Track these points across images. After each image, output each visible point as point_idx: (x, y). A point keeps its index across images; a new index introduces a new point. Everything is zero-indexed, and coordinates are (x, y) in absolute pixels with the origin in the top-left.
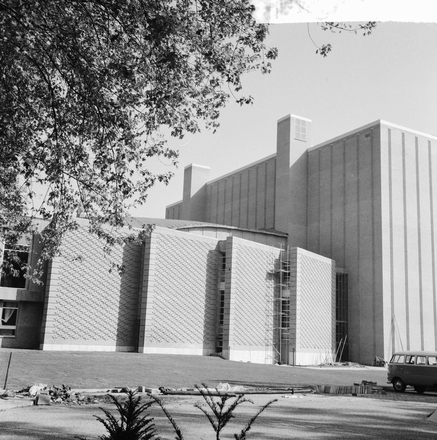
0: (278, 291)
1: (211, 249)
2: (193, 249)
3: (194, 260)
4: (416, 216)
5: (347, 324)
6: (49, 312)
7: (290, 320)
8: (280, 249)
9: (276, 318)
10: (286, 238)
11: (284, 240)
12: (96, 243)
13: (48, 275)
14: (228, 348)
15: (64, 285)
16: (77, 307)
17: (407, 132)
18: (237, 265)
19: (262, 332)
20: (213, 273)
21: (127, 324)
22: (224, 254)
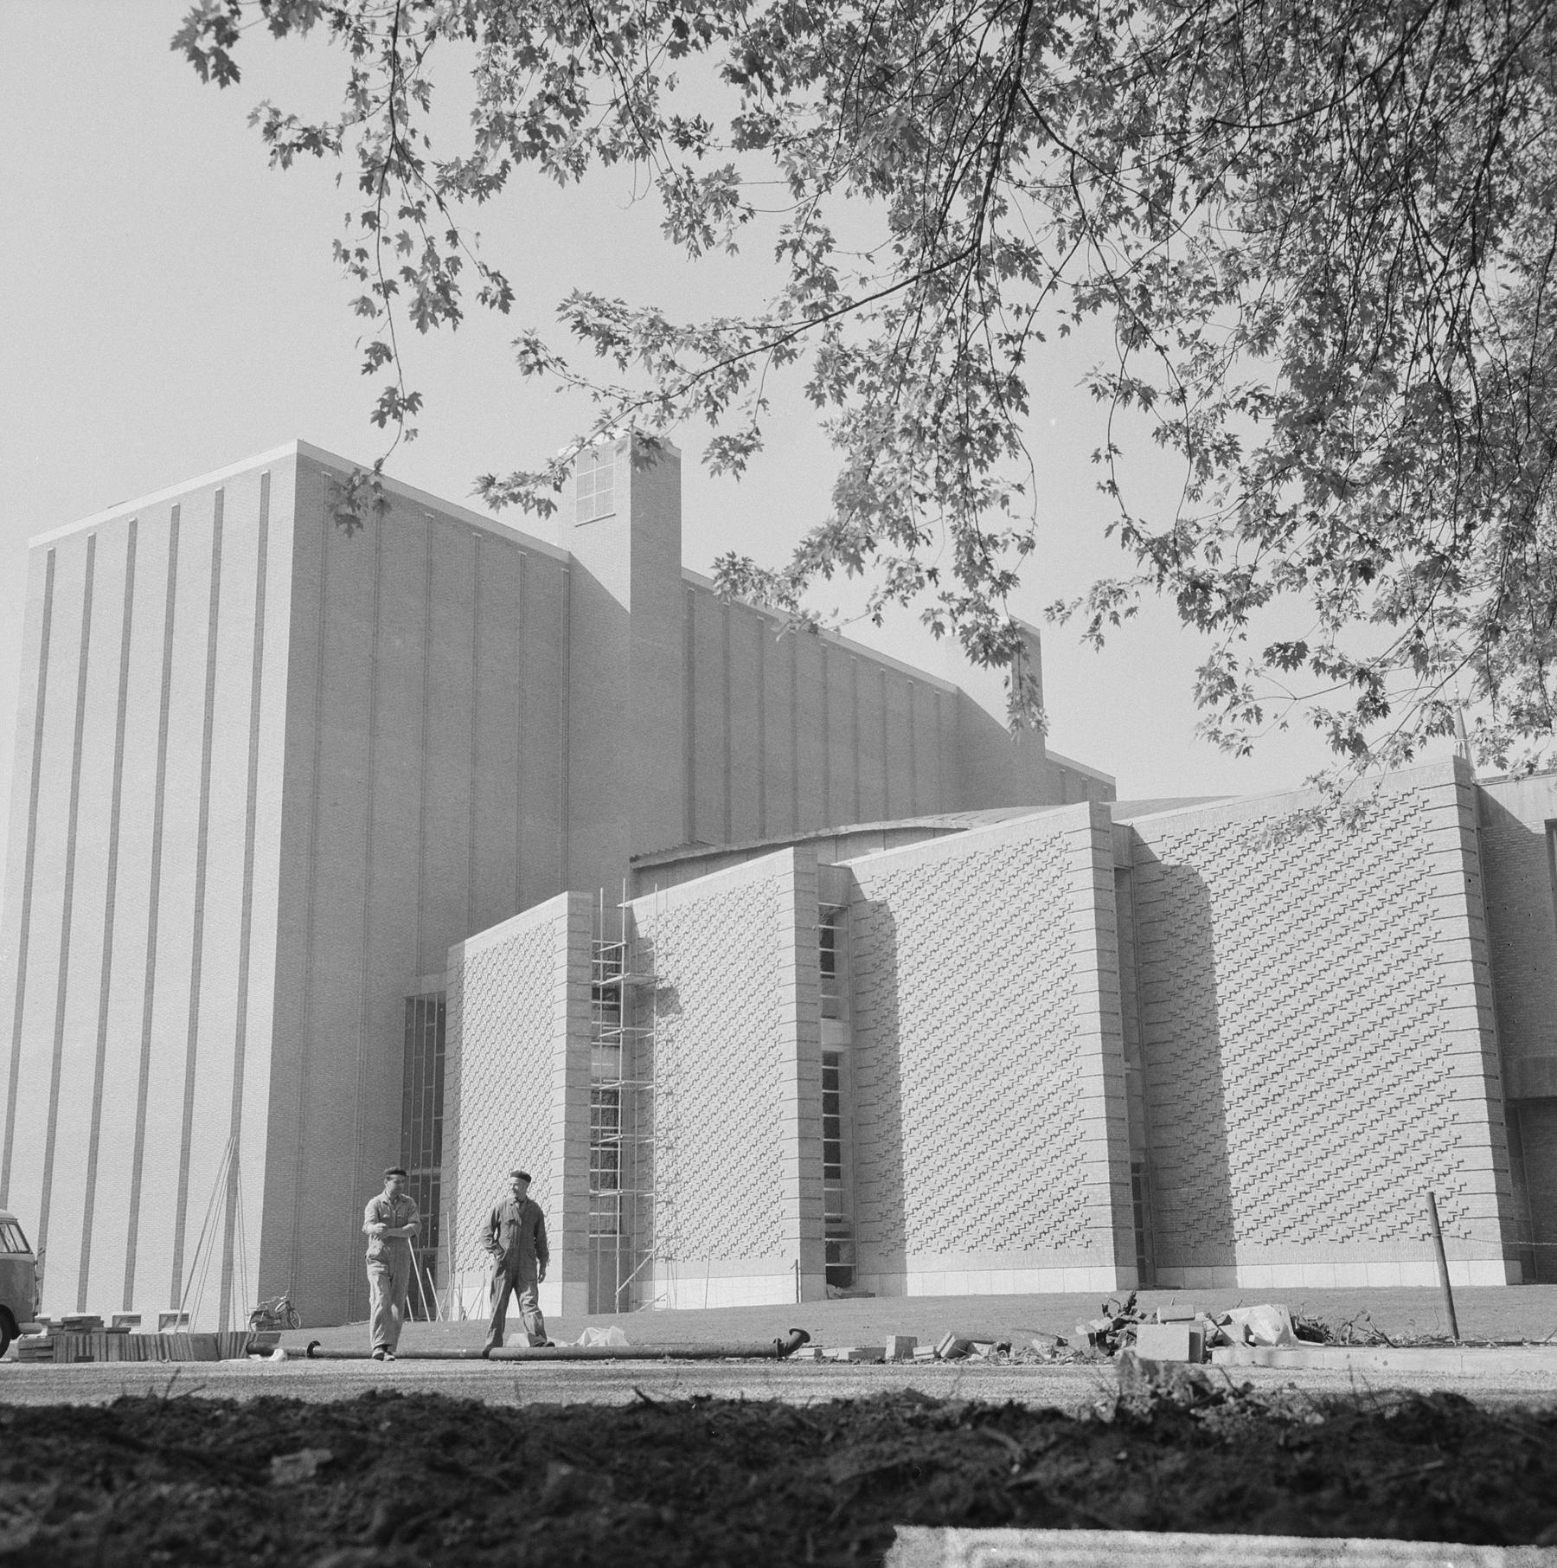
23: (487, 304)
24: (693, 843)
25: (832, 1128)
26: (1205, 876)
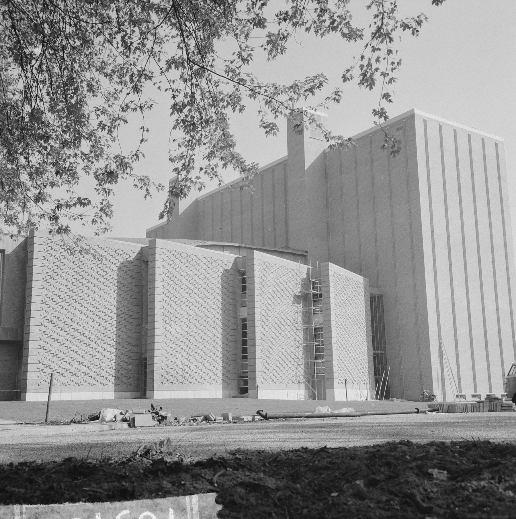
0: (307, 316)
1: (227, 268)
2: (205, 268)
3: (208, 282)
4: (459, 222)
5: (385, 354)
6: (31, 352)
7: (325, 350)
8: (307, 266)
9: (307, 349)
10: (305, 256)
11: (303, 258)
12: (86, 263)
13: (27, 306)
14: (255, 388)
15: (48, 317)
16: (67, 344)
17: (444, 123)
18: (260, 285)
19: (292, 367)
20: (231, 297)
21: (130, 364)
22: (243, 274)
23: (350, 80)
24: (287, 247)
25: (245, 343)
26: (118, 264)
